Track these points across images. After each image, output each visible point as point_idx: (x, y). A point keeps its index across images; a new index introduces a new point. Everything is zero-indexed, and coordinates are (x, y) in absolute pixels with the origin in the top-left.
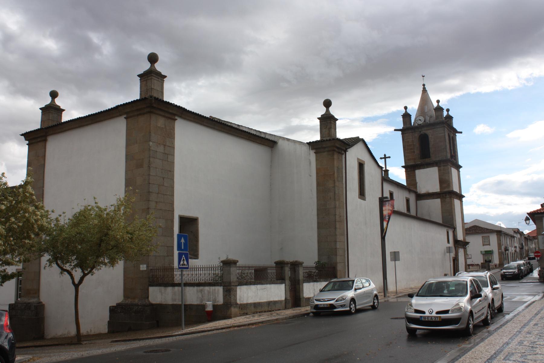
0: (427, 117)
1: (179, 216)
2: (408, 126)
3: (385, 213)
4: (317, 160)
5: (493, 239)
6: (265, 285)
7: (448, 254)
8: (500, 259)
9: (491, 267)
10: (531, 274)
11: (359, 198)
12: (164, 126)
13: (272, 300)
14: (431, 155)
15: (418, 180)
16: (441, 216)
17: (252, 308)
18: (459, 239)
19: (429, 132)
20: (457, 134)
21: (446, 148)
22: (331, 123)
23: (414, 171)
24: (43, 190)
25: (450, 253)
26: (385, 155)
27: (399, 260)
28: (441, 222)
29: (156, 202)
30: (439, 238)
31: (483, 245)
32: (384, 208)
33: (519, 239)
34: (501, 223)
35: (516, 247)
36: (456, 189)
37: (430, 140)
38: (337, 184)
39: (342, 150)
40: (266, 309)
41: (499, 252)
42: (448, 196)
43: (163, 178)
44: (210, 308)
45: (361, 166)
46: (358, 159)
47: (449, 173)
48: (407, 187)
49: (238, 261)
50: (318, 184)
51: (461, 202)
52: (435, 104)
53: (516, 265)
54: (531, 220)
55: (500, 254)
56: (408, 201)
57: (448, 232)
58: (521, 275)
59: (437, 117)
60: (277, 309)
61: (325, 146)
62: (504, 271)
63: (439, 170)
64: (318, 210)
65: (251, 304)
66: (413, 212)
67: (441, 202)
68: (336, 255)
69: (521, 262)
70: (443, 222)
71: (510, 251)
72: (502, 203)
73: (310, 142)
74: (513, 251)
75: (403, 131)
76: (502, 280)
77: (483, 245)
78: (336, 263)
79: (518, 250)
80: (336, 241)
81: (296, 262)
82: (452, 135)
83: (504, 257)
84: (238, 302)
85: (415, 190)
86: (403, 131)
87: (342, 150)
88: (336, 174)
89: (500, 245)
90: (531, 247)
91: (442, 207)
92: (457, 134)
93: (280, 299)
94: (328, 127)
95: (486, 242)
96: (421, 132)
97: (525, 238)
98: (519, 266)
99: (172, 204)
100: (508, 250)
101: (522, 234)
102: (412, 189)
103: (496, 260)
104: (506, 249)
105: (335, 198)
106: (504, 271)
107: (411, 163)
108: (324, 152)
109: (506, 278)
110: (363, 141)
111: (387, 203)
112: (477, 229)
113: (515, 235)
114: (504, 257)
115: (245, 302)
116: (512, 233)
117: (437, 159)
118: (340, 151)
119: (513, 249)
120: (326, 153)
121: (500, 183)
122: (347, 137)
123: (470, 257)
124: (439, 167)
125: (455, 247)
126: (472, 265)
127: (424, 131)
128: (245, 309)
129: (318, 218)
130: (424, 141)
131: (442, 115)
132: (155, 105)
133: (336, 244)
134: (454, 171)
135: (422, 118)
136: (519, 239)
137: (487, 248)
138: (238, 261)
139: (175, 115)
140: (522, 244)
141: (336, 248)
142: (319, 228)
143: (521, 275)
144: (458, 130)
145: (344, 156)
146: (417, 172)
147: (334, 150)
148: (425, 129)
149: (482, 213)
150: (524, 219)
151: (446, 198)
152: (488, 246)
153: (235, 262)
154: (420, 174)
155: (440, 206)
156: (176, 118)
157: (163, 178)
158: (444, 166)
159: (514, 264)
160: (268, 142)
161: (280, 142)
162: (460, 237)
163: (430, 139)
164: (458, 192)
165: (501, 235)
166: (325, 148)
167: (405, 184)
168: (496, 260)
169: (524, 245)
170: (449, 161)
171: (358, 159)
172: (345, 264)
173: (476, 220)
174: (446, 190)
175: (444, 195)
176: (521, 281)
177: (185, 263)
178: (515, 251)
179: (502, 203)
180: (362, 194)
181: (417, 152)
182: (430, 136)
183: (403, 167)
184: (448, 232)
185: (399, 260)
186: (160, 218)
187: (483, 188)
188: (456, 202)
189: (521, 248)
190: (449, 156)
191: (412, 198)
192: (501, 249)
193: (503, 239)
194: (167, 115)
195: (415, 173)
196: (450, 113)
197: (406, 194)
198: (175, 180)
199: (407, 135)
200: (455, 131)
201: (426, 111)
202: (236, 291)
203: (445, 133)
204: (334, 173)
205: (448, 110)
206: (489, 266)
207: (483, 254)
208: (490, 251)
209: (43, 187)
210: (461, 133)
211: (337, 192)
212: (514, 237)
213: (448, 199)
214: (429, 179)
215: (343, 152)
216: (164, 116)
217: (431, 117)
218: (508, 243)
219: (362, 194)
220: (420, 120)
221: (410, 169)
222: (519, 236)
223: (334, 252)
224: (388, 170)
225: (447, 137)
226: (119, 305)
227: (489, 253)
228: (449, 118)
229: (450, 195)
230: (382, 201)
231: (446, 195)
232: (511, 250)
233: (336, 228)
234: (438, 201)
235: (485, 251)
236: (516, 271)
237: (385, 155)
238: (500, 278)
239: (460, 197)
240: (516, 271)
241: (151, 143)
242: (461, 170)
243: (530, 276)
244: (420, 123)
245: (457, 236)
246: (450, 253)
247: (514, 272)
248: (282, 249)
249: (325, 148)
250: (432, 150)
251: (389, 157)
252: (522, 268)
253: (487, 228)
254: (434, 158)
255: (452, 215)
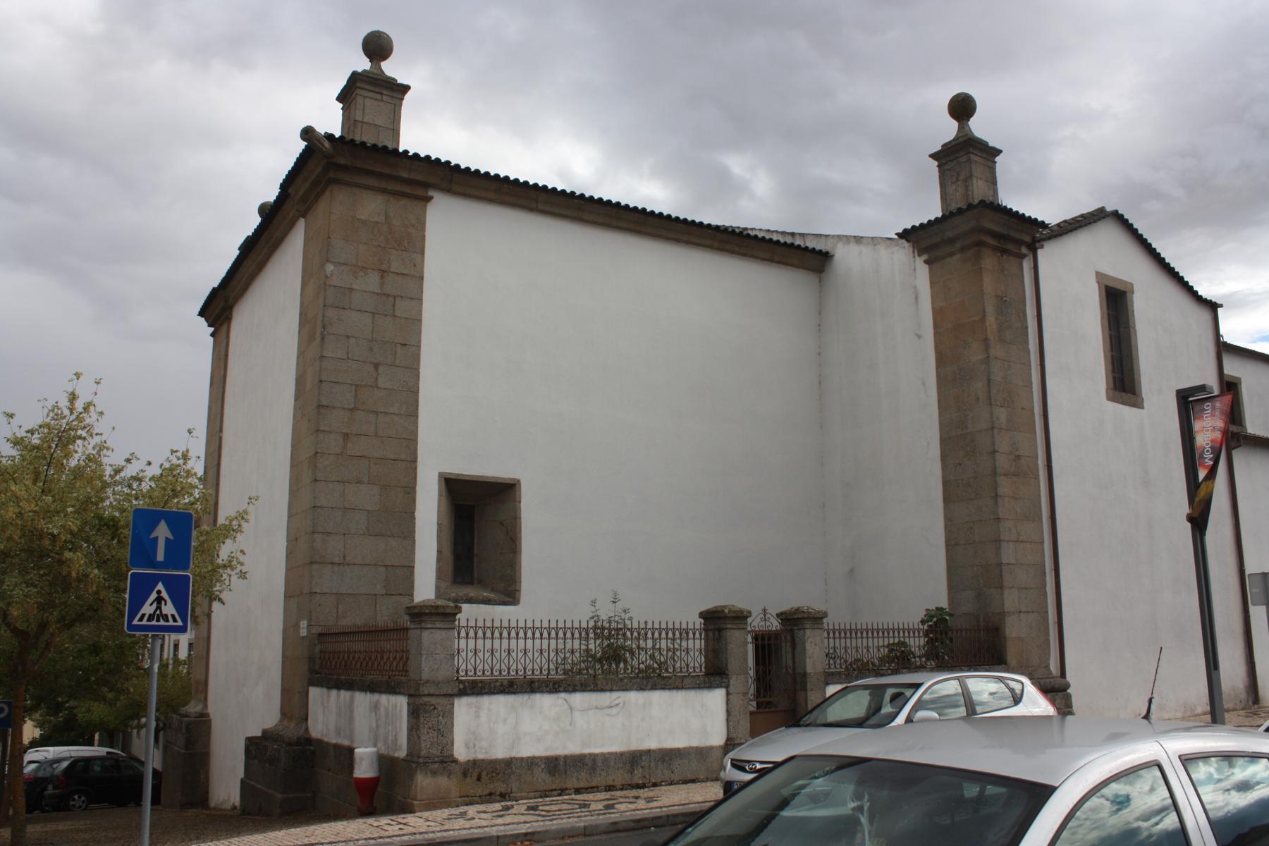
1: (441, 475)
4: (932, 284)
6: (615, 695)
12: (382, 219)
13: (653, 744)
17: (542, 778)
22: (969, 161)
24: (221, 438)
29: (346, 436)
32: (1197, 426)
38: (997, 351)
39: (1020, 243)
40: (619, 777)
43: (376, 366)
44: (364, 769)
45: (1116, 301)
46: (1099, 276)
49: (825, 615)
50: (941, 360)
60: (675, 777)
61: (950, 234)
64: (944, 441)
65: (531, 762)
68: (1001, 587)
73: (905, 230)
78: (1002, 615)
80: (998, 541)
81: (798, 610)
84: (461, 752)
87: (1020, 243)
88: (991, 320)
93: (695, 743)
94: (962, 177)
99: (411, 441)
105: (990, 398)
108: (951, 255)
110: (1118, 217)
115: (500, 753)
118: (1010, 246)
120: (958, 256)
122: (1068, 217)
128: (493, 779)
132: (342, 161)
133: (998, 549)
138: (825, 615)
139: (427, 186)
141: (1000, 564)
142: (947, 499)
145: (1027, 265)
147: (980, 244)
156: (431, 193)
157: (376, 366)
160: (802, 256)
161: (844, 257)
166: (952, 241)
171: (1099, 276)
172: (1046, 619)
177: (169, 609)
180: (1124, 382)
186: (359, 482)
194: (390, 186)
198: (421, 370)
202: (450, 714)
204: (983, 319)
209: (221, 430)
215: (1024, 250)
216: (384, 191)
219: (1124, 382)
226: (267, 735)
233: (996, 496)
241: (330, 268)
248: (852, 571)
249: (952, 241)
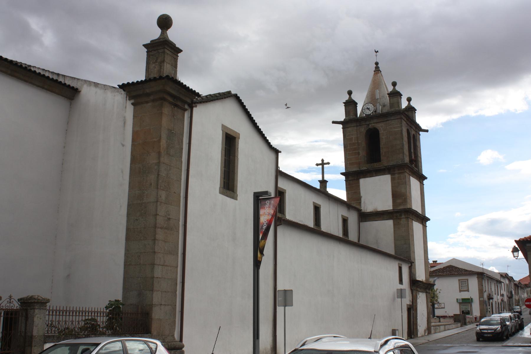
0: (378, 105)
2: (352, 117)
3: (264, 219)
5: (473, 282)
7: (400, 299)
8: (482, 311)
9: (468, 320)
10: (521, 332)
11: (220, 193)
14: (382, 158)
15: (362, 193)
16: (393, 245)
18: (418, 279)
19: (381, 127)
20: (421, 133)
21: (402, 148)
22: (164, 52)
23: (358, 180)
25: (401, 298)
26: (323, 160)
27: (292, 305)
28: (392, 252)
30: (386, 275)
31: (460, 291)
32: (262, 212)
33: (507, 285)
34: (494, 268)
35: (502, 295)
36: (416, 206)
37: (383, 140)
38: (164, 159)
39: (185, 102)
41: (480, 301)
42: (403, 216)
45: (230, 141)
46: (223, 127)
47: (407, 184)
48: (348, 203)
49: (48, 301)
51: (425, 227)
52: (390, 88)
53: (499, 318)
54: (520, 252)
55: (482, 303)
56: (345, 221)
57: (400, 269)
58: (506, 333)
59: (392, 105)
61: (148, 91)
62: (482, 327)
63: (393, 180)
66: (353, 236)
67: (394, 225)
68: (152, 290)
69: (507, 315)
70: (396, 252)
71: (495, 299)
72: (496, 246)
74: (500, 301)
75: (345, 124)
76: (478, 340)
77: (460, 291)
78: (151, 306)
79: (506, 299)
80: (153, 265)
81: (32, 298)
82: (413, 132)
83: (487, 306)
85: (357, 207)
86: (345, 124)
87: (185, 102)
89: (481, 292)
90: (522, 296)
91: (394, 230)
92: (421, 133)
94: (159, 61)
95: (464, 287)
96: (369, 125)
97: (515, 285)
98: (503, 321)
100: (492, 299)
101: (511, 279)
102: (354, 205)
103: (476, 311)
104: (490, 298)
106: (482, 327)
107: (355, 169)
108: (147, 102)
109: (483, 338)
110: (237, 98)
111: (268, 202)
112: (452, 270)
113: (502, 280)
114: (487, 306)
116: (498, 278)
117: (391, 163)
118: (179, 103)
119: (499, 297)
120: (150, 104)
121: (493, 222)
123: (443, 306)
124: (392, 174)
125: (412, 290)
126: (444, 317)
127: (373, 124)
129: (128, 221)
130: (373, 139)
131: (399, 103)
133: (153, 269)
134: (414, 182)
135: (371, 106)
136: (507, 285)
137: (465, 295)
138: (48, 301)
140: (511, 292)
141: (153, 278)
142: (128, 238)
143: (506, 333)
144: (423, 127)
145: (187, 115)
146: (362, 181)
147: (164, 99)
148: (375, 121)
149: (472, 256)
150: (511, 250)
151: (400, 219)
152: (467, 292)
153: (42, 303)
154: (367, 185)
155: (393, 230)
158: (399, 173)
159: (496, 317)
161: (86, 92)
162: (421, 275)
163: (381, 136)
164: (420, 211)
165: (483, 278)
166: (148, 95)
167: (345, 200)
168: (476, 311)
169: (513, 293)
170: (410, 166)
171: (223, 127)
172: (175, 309)
173: (454, 260)
174: (401, 207)
175: (398, 214)
176: (505, 344)
178: (502, 300)
179: (496, 246)
180: (229, 185)
181: (363, 153)
182: (381, 132)
183: (342, 174)
184: (400, 269)
185: (292, 305)
187: (472, 228)
188: (417, 226)
189: (510, 297)
190: (407, 160)
191: (353, 218)
192: (483, 297)
193: (485, 284)
195: (359, 183)
196: (412, 104)
197: (343, 212)
199: (349, 129)
200: (418, 129)
201: (378, 96)
203: (402, 126)
204: (159, 141)
205: (409, 100)
206: (465, 319)
207: (460, 303)
208: (468, 299)
210: (427, 131)
211: (163, 173)
212: (500, 282)
213: (403, 221)
214: (377, 192)
215: (186, 107)
217: (384, 106)
218: (493, 289)
219: (229, 185)
220: (368, 109)
221: (352, 177)
222: (507, 282)
223: (148, 284)
224: (326, 182)
225: (405, 134)
227: (467, 302)
228: (411, 110)
229: (407, 216)
230: (259, 199)
231: (401, 215)
232: (497, 298)
233: (155, 239)
234: (389, 223)
235: (463, 299)
236: (499, 327)
237: (323, 160)
238: (475, 338)
239: (423, 220)
240: (499, 327)
242: (425, 182)
243: (519, 335)
244: (368, 112)
245: (415, 275)
246: (401, 298)
247: (495, 330)
248: (69, 276)
249: (148, 95)
250: (383, 151)
251: (328, 163)
252: (508, 323)
253: (466, 269)
254: (385, 162)
255: (409, 244)
